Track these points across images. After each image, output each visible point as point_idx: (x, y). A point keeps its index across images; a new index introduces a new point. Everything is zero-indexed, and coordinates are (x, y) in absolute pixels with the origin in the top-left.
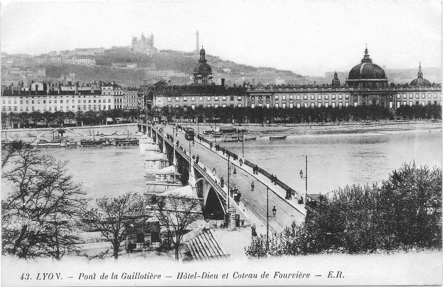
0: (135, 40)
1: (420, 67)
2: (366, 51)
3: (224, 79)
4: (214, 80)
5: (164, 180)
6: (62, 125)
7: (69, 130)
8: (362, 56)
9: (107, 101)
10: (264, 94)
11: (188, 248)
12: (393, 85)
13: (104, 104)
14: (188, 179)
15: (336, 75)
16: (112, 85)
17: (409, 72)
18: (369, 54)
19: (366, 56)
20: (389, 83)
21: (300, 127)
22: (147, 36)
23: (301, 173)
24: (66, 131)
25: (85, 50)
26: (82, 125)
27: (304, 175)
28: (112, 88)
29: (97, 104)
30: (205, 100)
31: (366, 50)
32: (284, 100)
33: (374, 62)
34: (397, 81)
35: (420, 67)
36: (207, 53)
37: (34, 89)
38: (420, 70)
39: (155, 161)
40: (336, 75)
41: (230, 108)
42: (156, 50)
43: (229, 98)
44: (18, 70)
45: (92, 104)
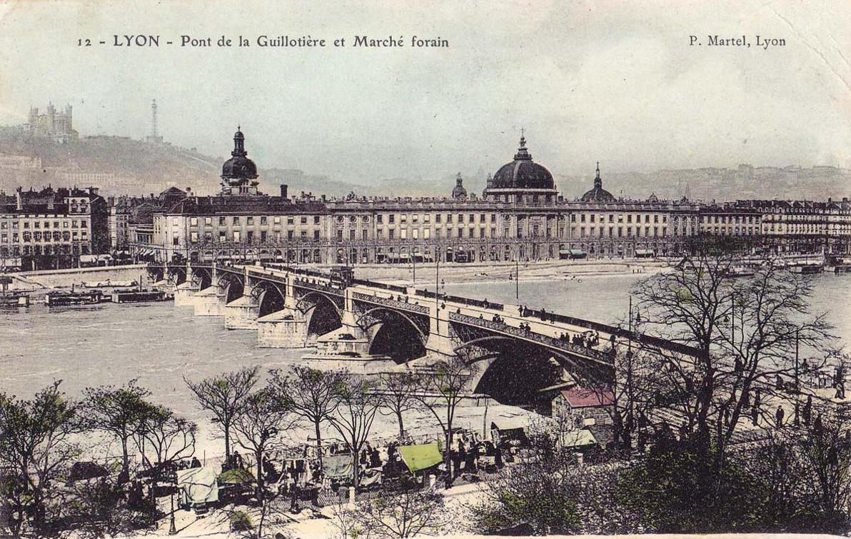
2: (523, 142)
3: (286, 186)
5: (334, 352)
7: (20, 278)
10: (347, 214)
16: (86, 195)
19: (240, 152)
21: (426, 270)
24: (13, 280)
31: (523, 139)
32: (193, 226)
33: (535, 161)
35: (598, 170)
39: (276, 323)
43: (216, 220)
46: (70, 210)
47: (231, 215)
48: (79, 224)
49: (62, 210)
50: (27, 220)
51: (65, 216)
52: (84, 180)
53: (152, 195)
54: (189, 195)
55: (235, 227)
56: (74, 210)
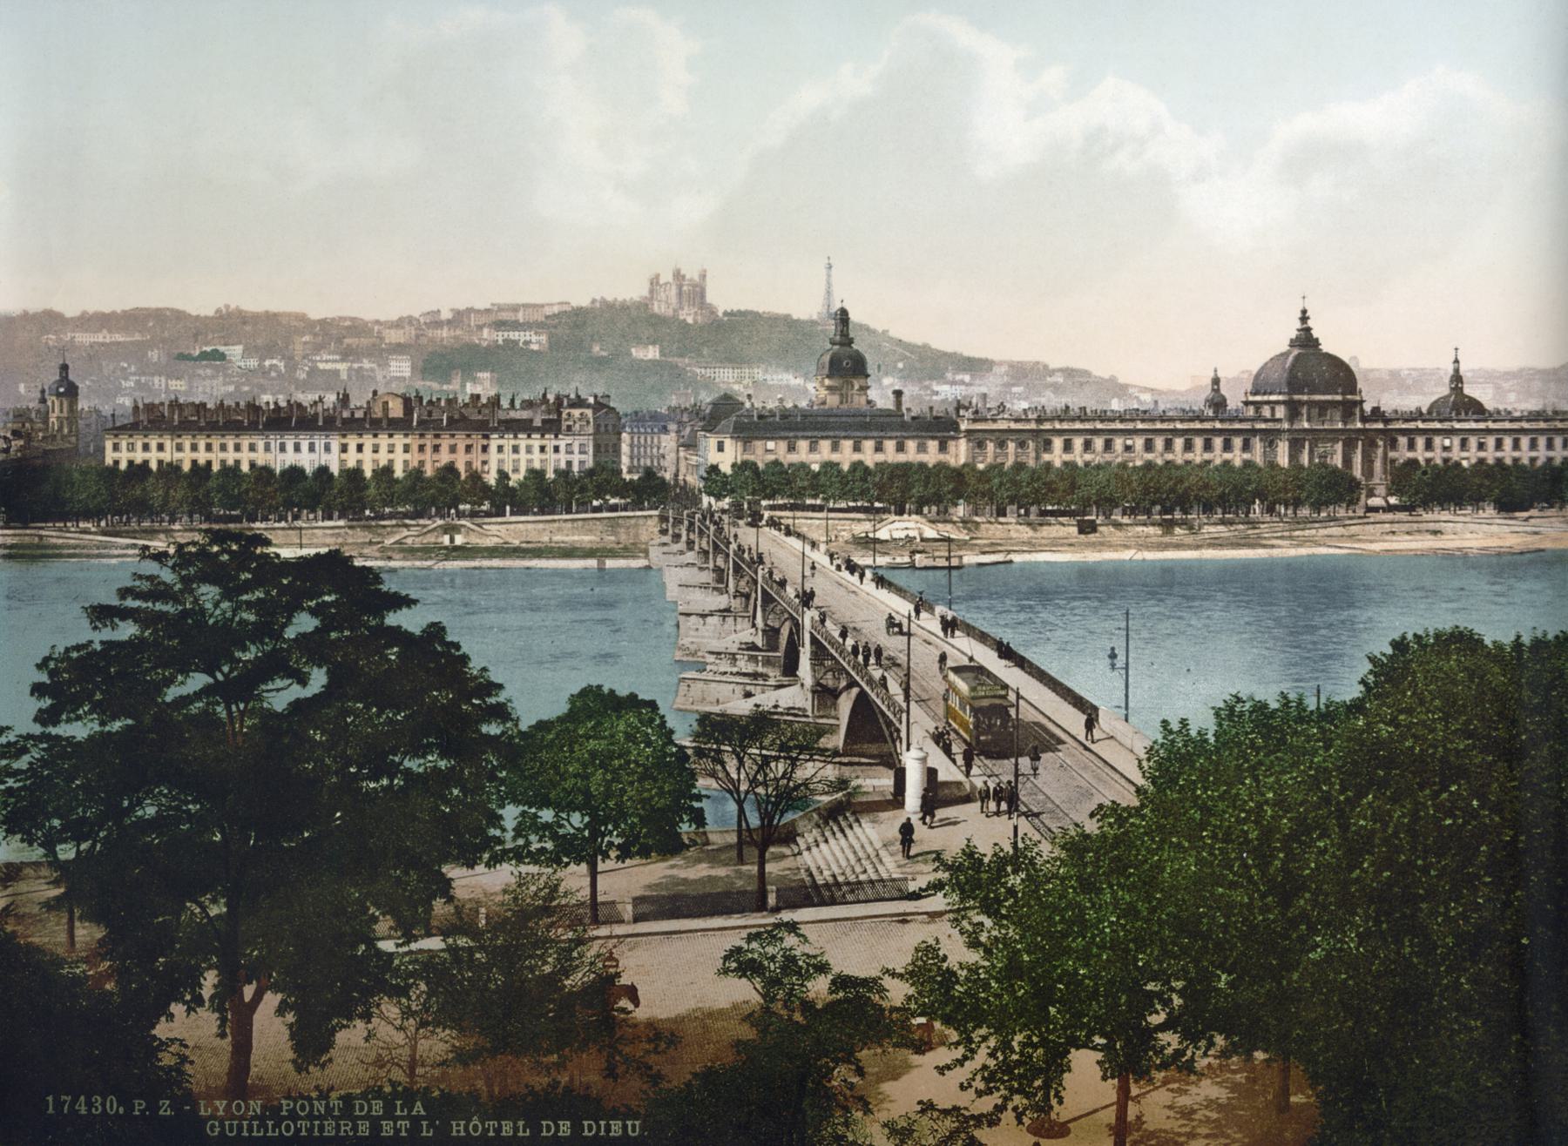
0: (654, 282)
1: (1457, 361)
2: (1304, 318)
4: (873, 394)
6: (453, 511)
8: (1292, 329)
9: (576, 449)
11: (501, 610)
12: (1377, 414)
13: (569, 457)
14: (796, 668)
15: (1216, 381)
16: (589, 406)
17: (1420, 379)
18: (1310, 323)
20: (1368, 407)
22: (691, 273)
23: (1113, 656)
25: (515, 309)
26: (508, 513)
27: (1120, 661)
28: (589, 412)
29: (523, 456)
30: (760, 451)
31: (1304, 312)
33: (1326, 347)
34: (1391, 402)
35: (1457, 361)
36: (854, 317)
37: (378, 412)
38: (1457, 371)
40: (1216, 381)
41: (903, 471)
42: (713, 312)
43: (783, 445)
44: (336, 361)
45: (536, 456)
46: (564, 427)
47: (806, 438)
48: (576, 449)
49: (552, 426)
50: (501, 442)
51: (556, 436)
52: (587, 386)
53: (931, 408)
54: (748, 405)
55: (1465, 454)
56: (569, 428)
